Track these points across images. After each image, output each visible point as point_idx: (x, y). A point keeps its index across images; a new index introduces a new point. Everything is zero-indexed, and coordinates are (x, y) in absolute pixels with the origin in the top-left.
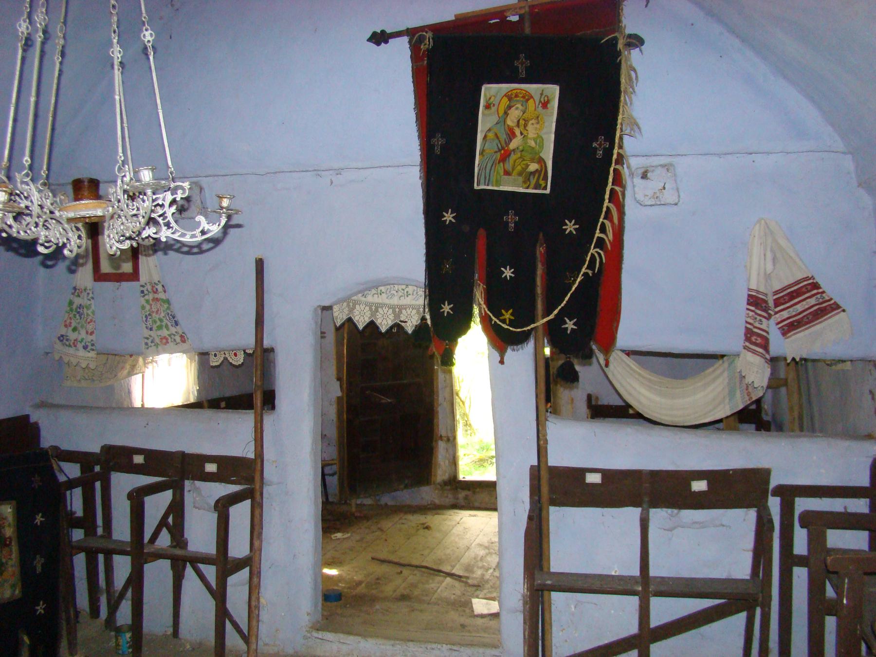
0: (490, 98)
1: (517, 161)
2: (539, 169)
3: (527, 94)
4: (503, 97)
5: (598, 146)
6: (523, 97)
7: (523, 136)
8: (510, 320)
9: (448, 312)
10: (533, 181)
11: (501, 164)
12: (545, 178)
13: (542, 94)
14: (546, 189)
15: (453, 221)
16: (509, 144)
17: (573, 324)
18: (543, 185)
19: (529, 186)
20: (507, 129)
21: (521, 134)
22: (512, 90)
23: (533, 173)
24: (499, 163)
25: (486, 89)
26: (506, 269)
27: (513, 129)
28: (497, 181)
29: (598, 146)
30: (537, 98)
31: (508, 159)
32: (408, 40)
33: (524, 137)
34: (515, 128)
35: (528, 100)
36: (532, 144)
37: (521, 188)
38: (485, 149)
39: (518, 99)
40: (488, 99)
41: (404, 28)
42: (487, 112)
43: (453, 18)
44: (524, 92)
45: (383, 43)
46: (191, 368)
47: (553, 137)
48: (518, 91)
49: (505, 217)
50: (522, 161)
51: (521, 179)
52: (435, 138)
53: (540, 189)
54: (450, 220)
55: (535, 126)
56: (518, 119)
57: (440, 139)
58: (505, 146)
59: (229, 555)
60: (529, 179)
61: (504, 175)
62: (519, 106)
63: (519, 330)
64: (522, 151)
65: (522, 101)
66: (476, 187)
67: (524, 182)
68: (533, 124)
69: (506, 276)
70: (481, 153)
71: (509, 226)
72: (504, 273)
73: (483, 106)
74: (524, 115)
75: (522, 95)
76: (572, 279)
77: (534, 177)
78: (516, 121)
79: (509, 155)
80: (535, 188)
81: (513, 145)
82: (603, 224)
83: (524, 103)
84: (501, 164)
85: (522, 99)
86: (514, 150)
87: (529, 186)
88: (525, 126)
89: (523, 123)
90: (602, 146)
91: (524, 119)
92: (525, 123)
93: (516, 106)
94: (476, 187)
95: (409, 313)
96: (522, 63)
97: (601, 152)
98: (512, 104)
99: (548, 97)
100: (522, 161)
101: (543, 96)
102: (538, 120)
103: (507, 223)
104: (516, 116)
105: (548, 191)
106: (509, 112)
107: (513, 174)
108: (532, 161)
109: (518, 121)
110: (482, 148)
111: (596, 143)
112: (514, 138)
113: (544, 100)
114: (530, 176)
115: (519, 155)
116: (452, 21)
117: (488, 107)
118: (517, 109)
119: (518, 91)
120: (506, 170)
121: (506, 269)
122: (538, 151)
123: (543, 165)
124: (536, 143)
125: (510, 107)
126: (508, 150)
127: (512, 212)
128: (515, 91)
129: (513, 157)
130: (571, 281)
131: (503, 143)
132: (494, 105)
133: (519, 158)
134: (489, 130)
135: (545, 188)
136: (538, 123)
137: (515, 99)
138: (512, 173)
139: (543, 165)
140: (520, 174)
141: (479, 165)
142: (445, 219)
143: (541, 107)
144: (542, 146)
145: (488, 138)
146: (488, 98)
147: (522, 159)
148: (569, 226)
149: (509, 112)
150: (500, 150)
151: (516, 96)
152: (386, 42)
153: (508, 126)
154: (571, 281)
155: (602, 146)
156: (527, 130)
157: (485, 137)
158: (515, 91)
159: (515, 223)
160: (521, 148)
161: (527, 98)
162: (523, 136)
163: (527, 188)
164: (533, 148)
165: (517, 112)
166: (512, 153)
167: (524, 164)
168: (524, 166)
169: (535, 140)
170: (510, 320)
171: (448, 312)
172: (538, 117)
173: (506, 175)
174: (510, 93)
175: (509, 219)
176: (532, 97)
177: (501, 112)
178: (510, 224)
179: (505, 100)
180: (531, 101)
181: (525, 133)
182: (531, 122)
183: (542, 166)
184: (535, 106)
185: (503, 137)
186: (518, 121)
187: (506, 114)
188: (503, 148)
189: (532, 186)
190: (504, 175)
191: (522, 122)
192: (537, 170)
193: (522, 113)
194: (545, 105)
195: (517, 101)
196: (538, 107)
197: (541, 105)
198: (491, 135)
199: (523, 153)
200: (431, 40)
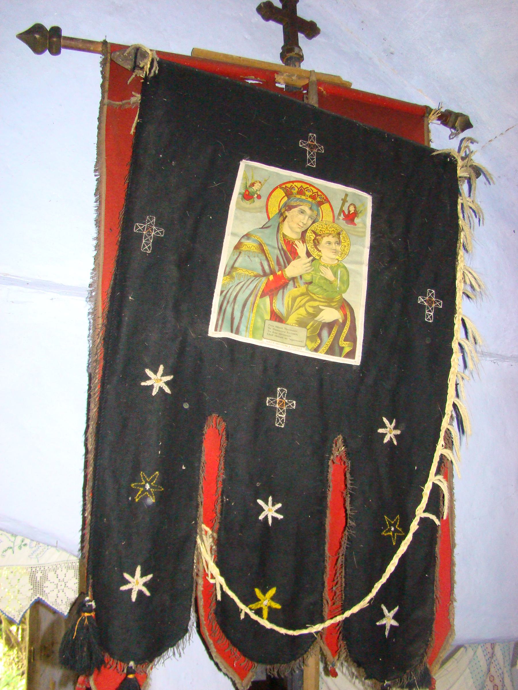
0: (253, 185)
1: (298, 300)
2: (341, 321)
3: (319, 193)
4: (277, 188)
5: (426, 304)
6: (313, 197)
7: (311, 258)
8: (271, 610)
9: (140, 593)
10: (327, 340)
11: (267, 299)
12: (352, 337)
13: (344, 201)
14: (353, 358)
15: (167, 390)
16: (285, 267)
17: (385, 624)
18: (347, 350)
19: (319, 346)
20: (281, 241)
21: (308, 254)
22: (293, 182)
23: (330, 326)
24: (262, 296)
25: (247, 166)
26: (267, 503)
27: (293, 243)
28: (255, 329)
29: (426, 304)
30: (337, 205)
31: (281, 291)
32: (101, 60)
33: (313, 261)
34: (297, 242)
35: (320, 204)
36: (329, 275)
37: (304, 349)
38: (236, 265)
39: (303, 197)
40: (248, 185)
41: (100, 39)
42: (246, 204)
43: (188, 53)
44: (315, 190)
45: (47, 52)
46: (231, 294)
47: (365, 270)
48: (305, 186)
49: (268, 399)
50: (308, 301)
51: (303, 333)
52: (145, 223)
53: (340, 356)
54: (160, 387)
55: (334, 246)
56: (303, 230)
57: (154, 228)
58: (277, 268)
59: (190, 54)
60: (319, 335)
61: (271, 319)
62: (307, 209)
63: (283, 631)
64: (311, 283)
65: (312, 203)
66: (212, 333)
67: (311, 338)
68: (329, 243)
69: (266, 517)
70: (229, 274)
71: (277, 417)
72: (263, 510)
73: (240, 194)
74: (315, 225)
75: (311, 194)
76: (393, 529)
77: (330, 333)
78: (300, 231)
79: (284, 286)
80: (331, 351)
81: (290, 271)
82: (448, 432)
83: (315, 207)
84: (267, 299)
85: (310, 200)
86: (294, 279)
87: (319, 346)
88: (316, 243)
89: (313, 238)
90: (434, 305)
91: (314, 232)
92: (315, 239)
93: (302, 207)
94: (212, 333)
95: (61, 577)
96: (312, 147)
97: (432, 314)
98: (293, 203)
99: (355, 207)
100: (308, 301)
101: (347, 205)
102: (339, 238)
103: (273, 410)
104: (301, 224)
105: (357, 361)
106: (287, 213)
107: (289, 321)
108: (329, 302)
109: (304, 233)
110: (232, 263)
111: (423, 298)
112: (294, 259)
113: (349, 212)
114: (321, 329)
115: (302, 288)
116: (187, 56)
117: (247, 196)
118: (302, 212)
119: (305, 186)
120: (276, 311)
121: (267, 503)
122: (340, 288)
123: (348, 314)
124: (335, 274)
125: (289, 207)
126: (282, 276)
127: (282, 391)
128: (299, 185)
129: (291, 291)
130: (391, 534)
131: (273, 264)
132: (259, 197)
133: (302, 295)
134: (247, 236)
135: (351, 354)
136: (339, 243)
137: (298, 196)
138: (288, 318)
139: (348, 314)
140: (302, 324)
141: (222, 292)
142: (148, 383)
143: (343, 219)
144: (346, 283)
145: (244, 248)
146: (249, 183)
147: (308, 298)
148: (388, 429)
149: (287, 213)
150: (265, 274)
151: (301, 192)
152: (55, 51)
153: (284, 236)
154: (391, 534)
155: (434, 305)
156: (320, 251)
157: (238, 247)
158: (299, 185)
159: (289, 412)
160: (308, 278)
161: (318, 199)
162: (311, 258)
163: (316, 350)
164: (331, 283)
165: (301, 216)
166: (291, 283)
167: (312, 307)
168: (311, 310)
169: (334, 270)
170: (271, 610)
171: (140, 593)
172: (339, 234)
173: (276, 320)
174: (289, 185)
175: (275, 402)
176: (327, 201)
177: (274, 210)
178: (278, 415)
179: (280, 193)
180: (325, 207)
181: (315, 253)
182: (325, 240)
183: (345, 315)
184: (334, 217)
185: (274, 253)
186: (304, 233)
187: (282, 216)
188: (273, 272)
189: (325, 347)
190: (271, 319)
191: (310, 235)
192: (335, 322)
193: (310, 222)
194: (350, 218)
195: (302, 201)
196: (338, 219)
197: (342, 216)
198: (250, 245)
199: (311, 287)
200: (155, 64)
